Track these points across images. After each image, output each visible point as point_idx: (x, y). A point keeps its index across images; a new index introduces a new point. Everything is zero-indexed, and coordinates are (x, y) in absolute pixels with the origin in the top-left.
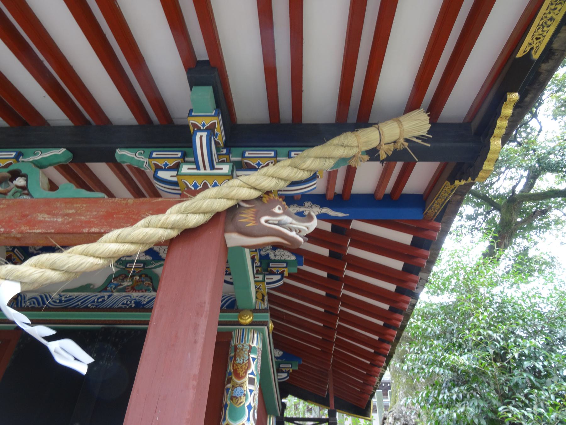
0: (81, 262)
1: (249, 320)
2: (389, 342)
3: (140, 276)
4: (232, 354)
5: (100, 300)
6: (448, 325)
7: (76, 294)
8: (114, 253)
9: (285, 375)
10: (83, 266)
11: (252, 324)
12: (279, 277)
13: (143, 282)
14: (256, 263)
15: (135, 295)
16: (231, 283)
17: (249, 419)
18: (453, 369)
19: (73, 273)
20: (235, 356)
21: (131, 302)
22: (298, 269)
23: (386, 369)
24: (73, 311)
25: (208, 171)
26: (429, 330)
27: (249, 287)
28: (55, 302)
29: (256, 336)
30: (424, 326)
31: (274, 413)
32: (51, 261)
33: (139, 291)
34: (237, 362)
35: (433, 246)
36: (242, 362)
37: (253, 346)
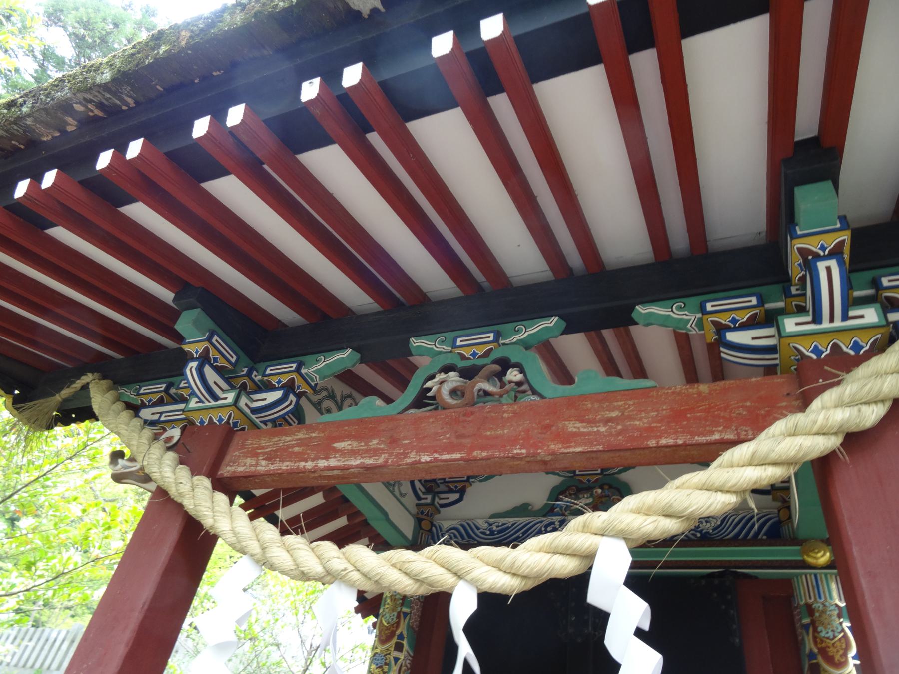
0: (709, 503)
7: (512, 520)
8: (755, 483)
12: (277, 395)
25: (838, 323)
28: (484, 533)
34: (823, 634)
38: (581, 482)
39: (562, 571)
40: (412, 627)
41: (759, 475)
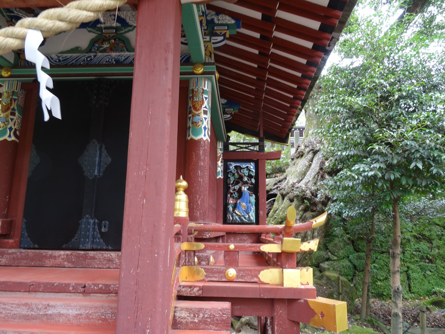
1: (201, 70)
2: (305, 89)
3: (115, 40)
4: (191, 95)
5: (88, 59)
6: (352, 77)
7: (69, 55)
8: (100, 7)
9: (229, 116)
10: (80, 18)
11: (203, 73)
12: (222, 38)
13: (118, 44)
14: (203, 26)
15: (114, 54)
16: (186, 44)
17: (205, 135)
18: (350, 108)
19: (75, 23)
20: (193, 96)
21: (112, 60)
22: (237, 32)
23: (301, 110)
24: (71, 67)
26: (337, 81)
27: (199, 45)
29: (206, 82)
30: (333, 79)
31: (222, 140)
32: (57, 14)
33: (116, 52)
34: (195, 100)
35: (346, 8)
36: (198, 100)
37: (205, 89)
38: (106, 37)
39: (12, 45)
40: (20, 106)
41: (102, 3)
